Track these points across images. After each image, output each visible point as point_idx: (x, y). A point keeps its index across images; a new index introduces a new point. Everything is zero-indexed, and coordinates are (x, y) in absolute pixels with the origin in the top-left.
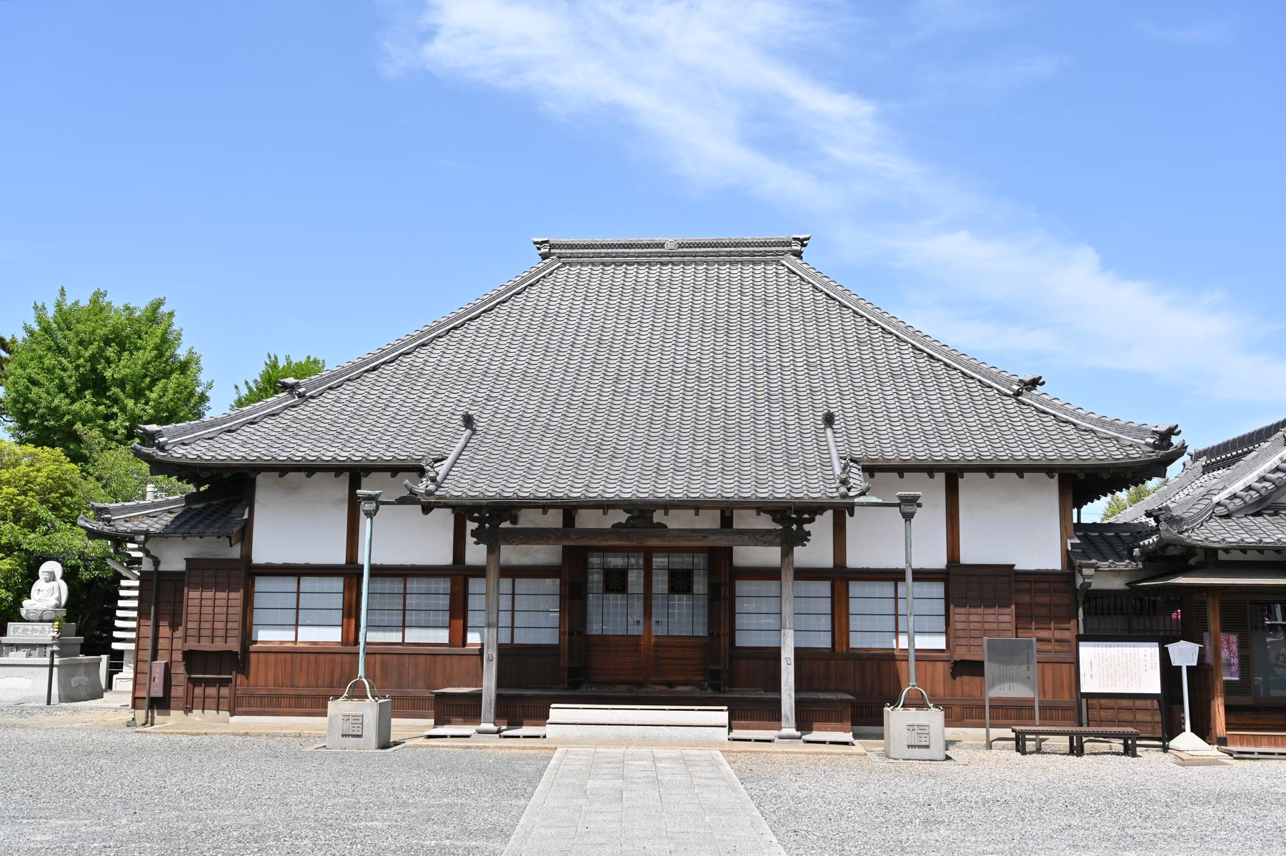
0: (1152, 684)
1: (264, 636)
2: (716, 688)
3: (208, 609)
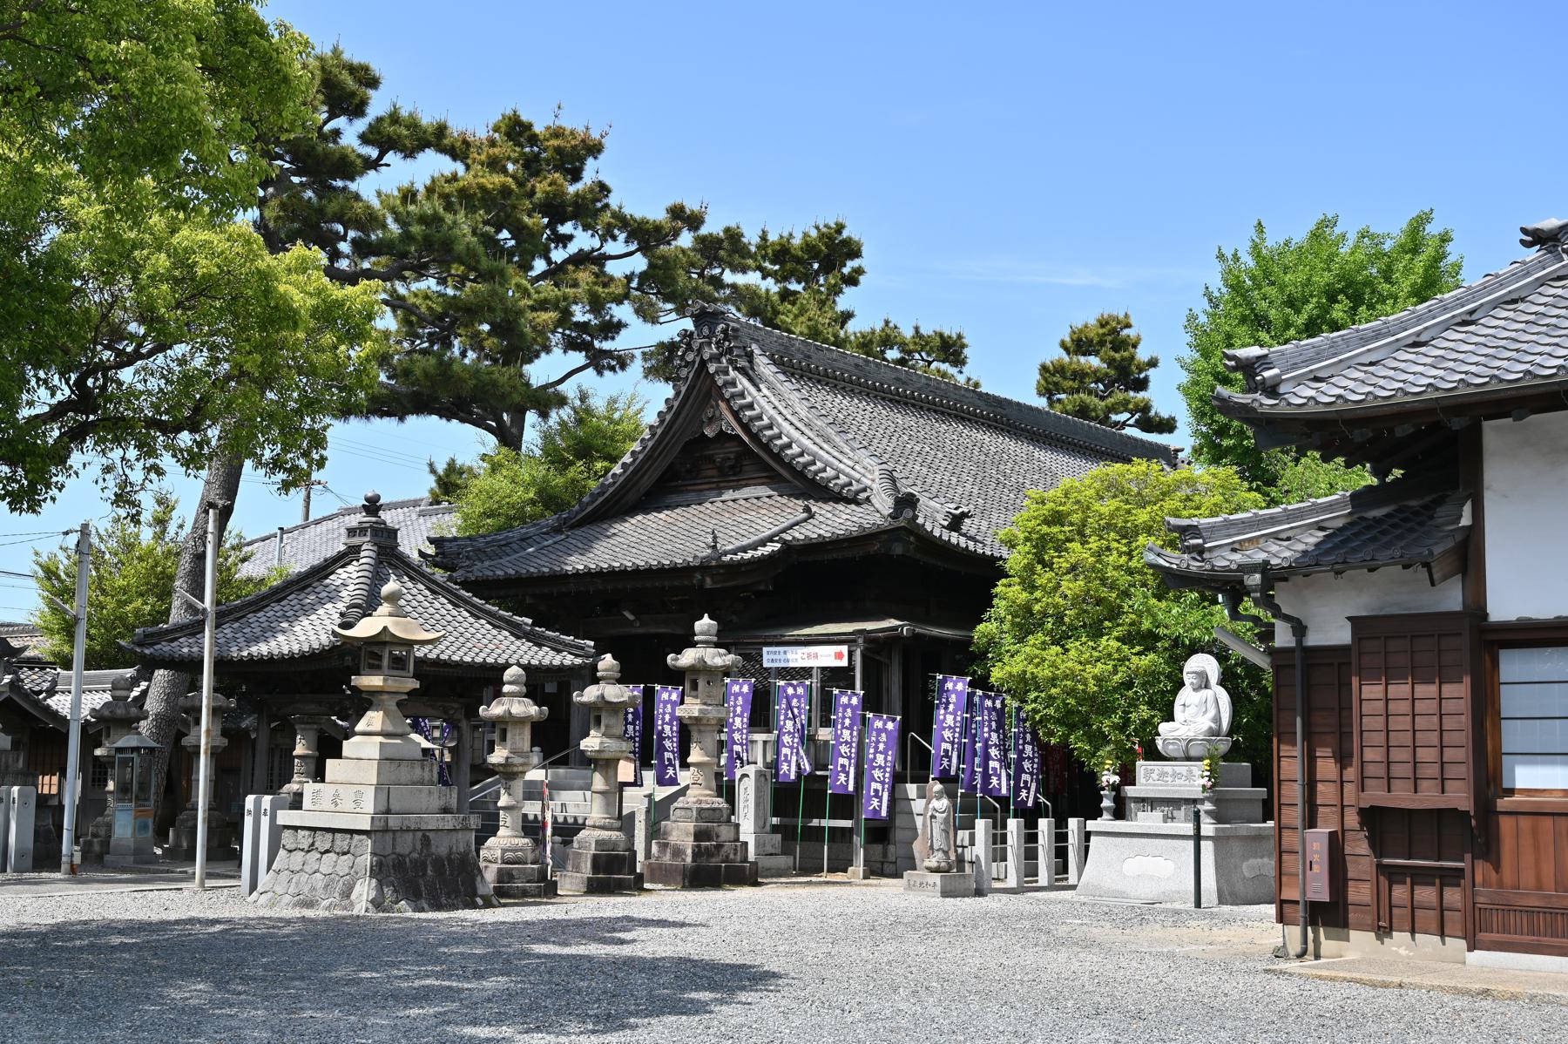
1: (1526, 777)
3: (1404, 717)
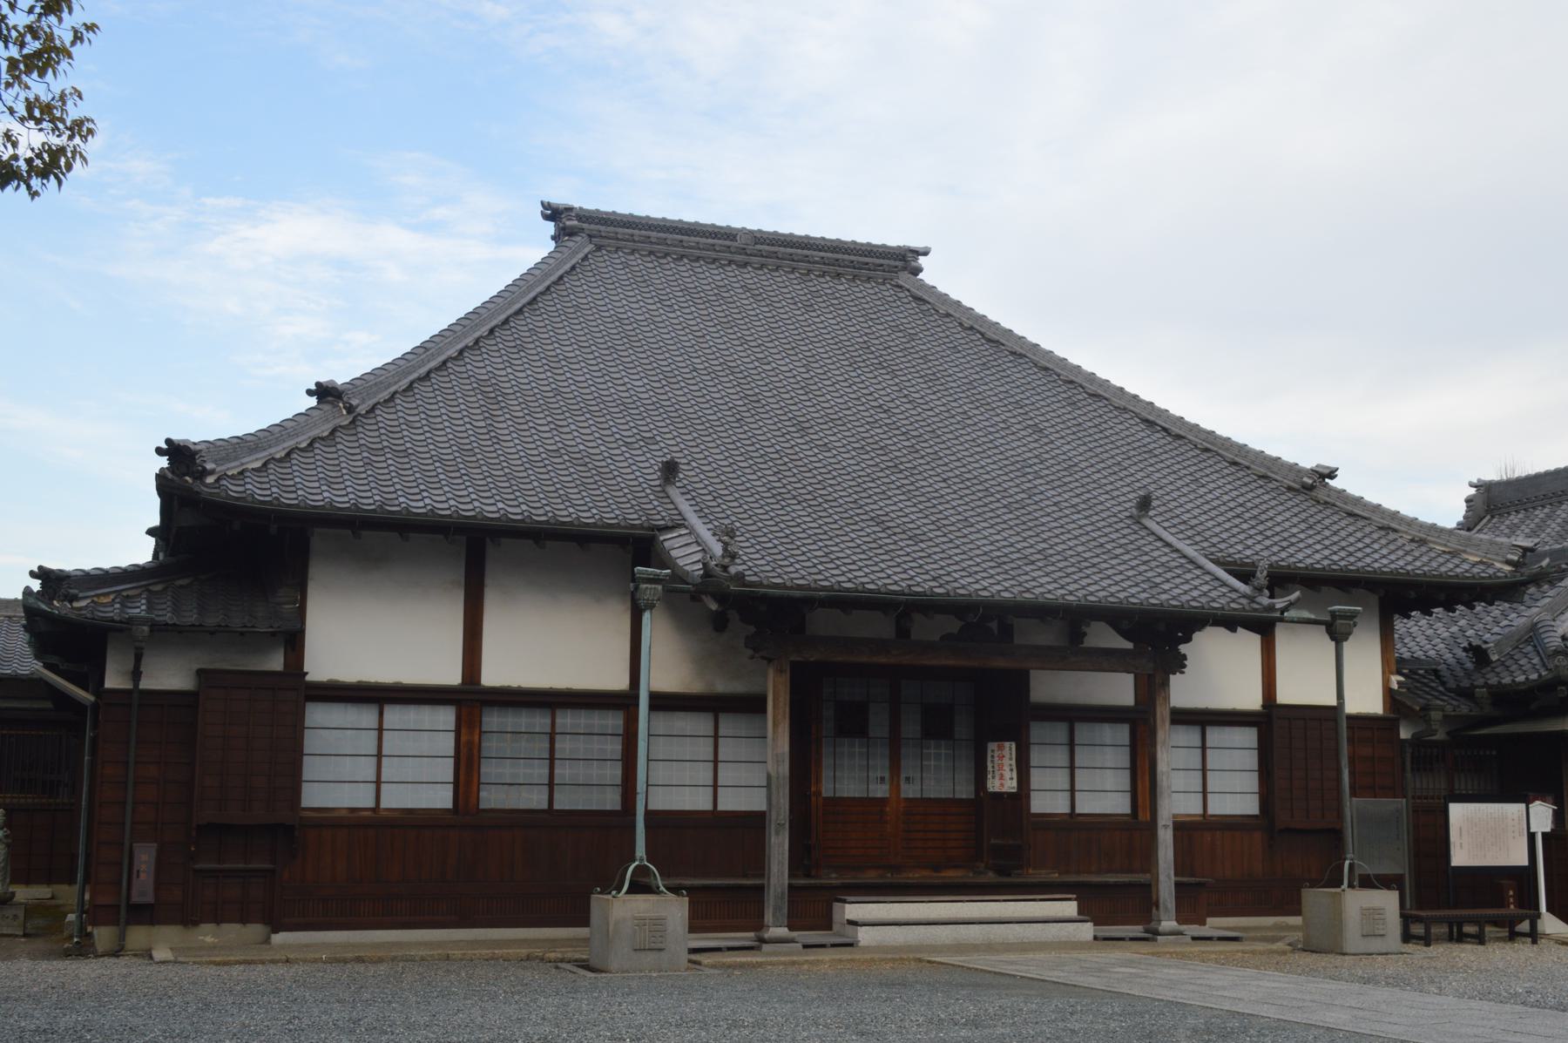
2: (1001, 871)
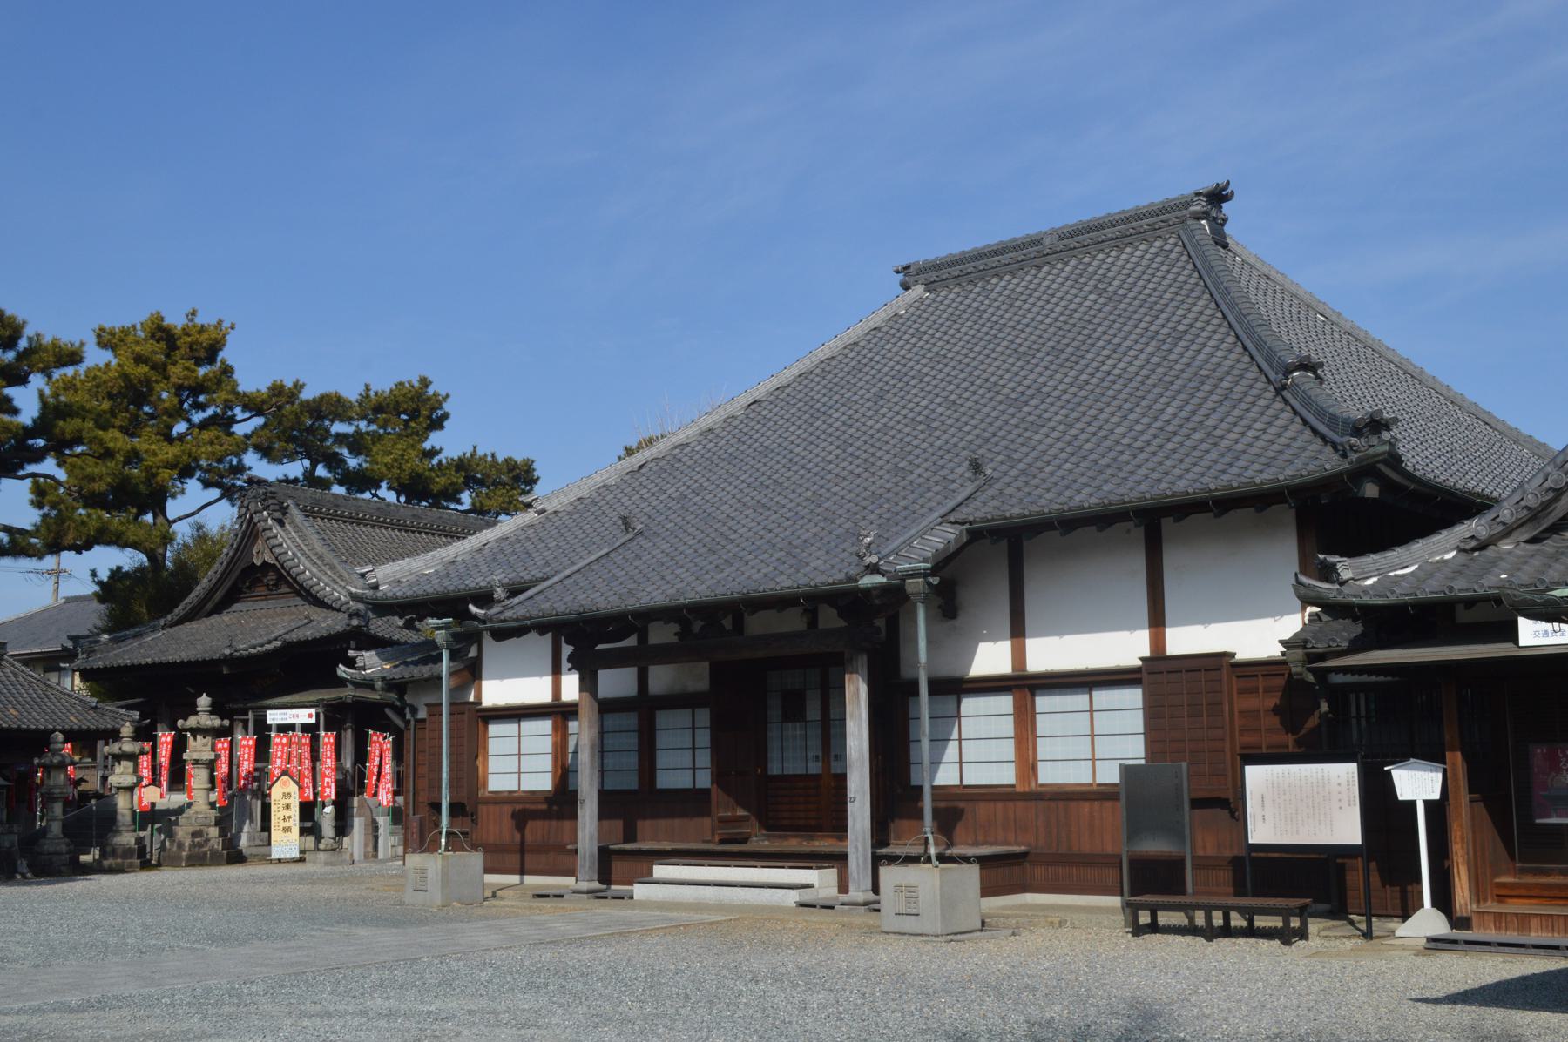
0: (1347, 829)
